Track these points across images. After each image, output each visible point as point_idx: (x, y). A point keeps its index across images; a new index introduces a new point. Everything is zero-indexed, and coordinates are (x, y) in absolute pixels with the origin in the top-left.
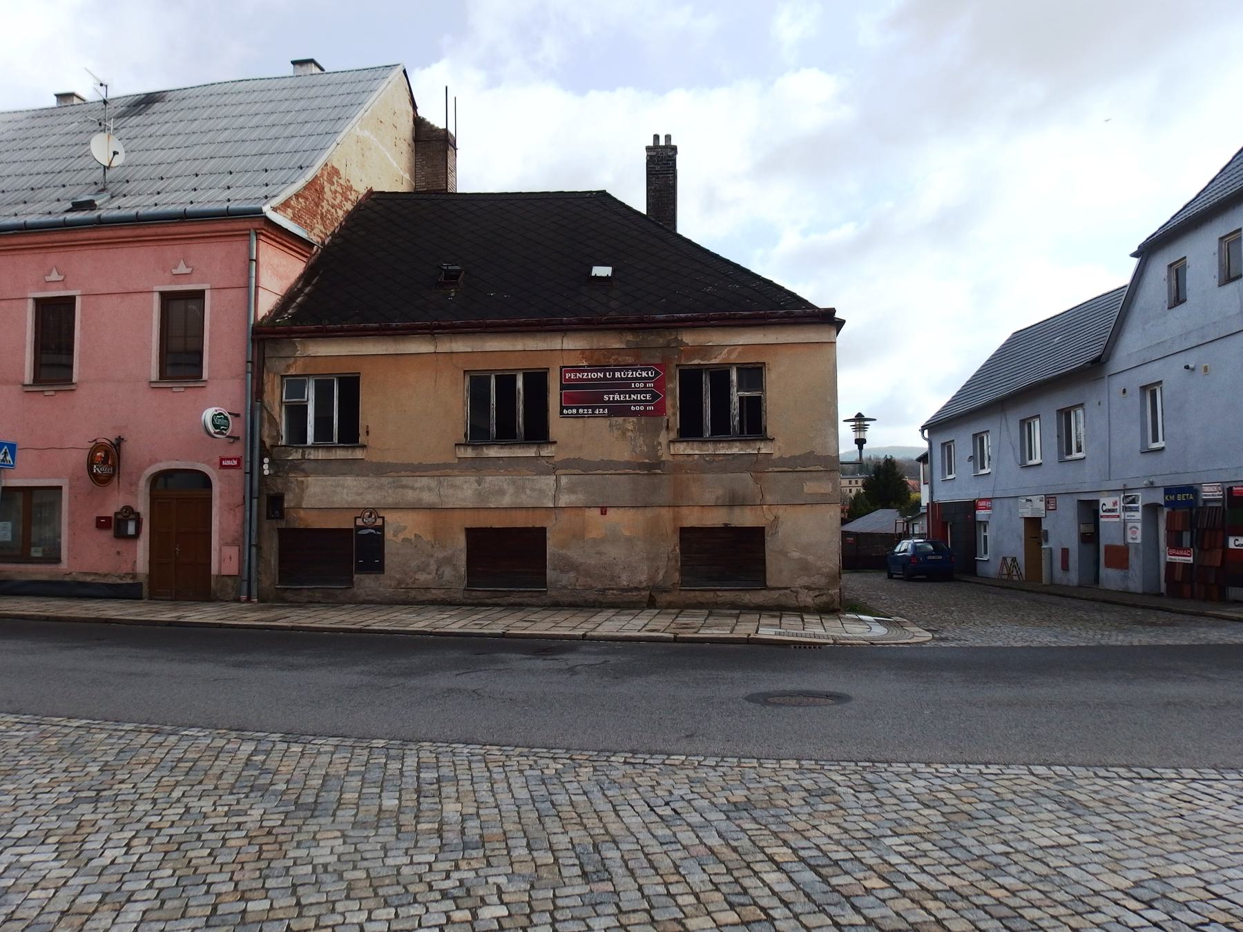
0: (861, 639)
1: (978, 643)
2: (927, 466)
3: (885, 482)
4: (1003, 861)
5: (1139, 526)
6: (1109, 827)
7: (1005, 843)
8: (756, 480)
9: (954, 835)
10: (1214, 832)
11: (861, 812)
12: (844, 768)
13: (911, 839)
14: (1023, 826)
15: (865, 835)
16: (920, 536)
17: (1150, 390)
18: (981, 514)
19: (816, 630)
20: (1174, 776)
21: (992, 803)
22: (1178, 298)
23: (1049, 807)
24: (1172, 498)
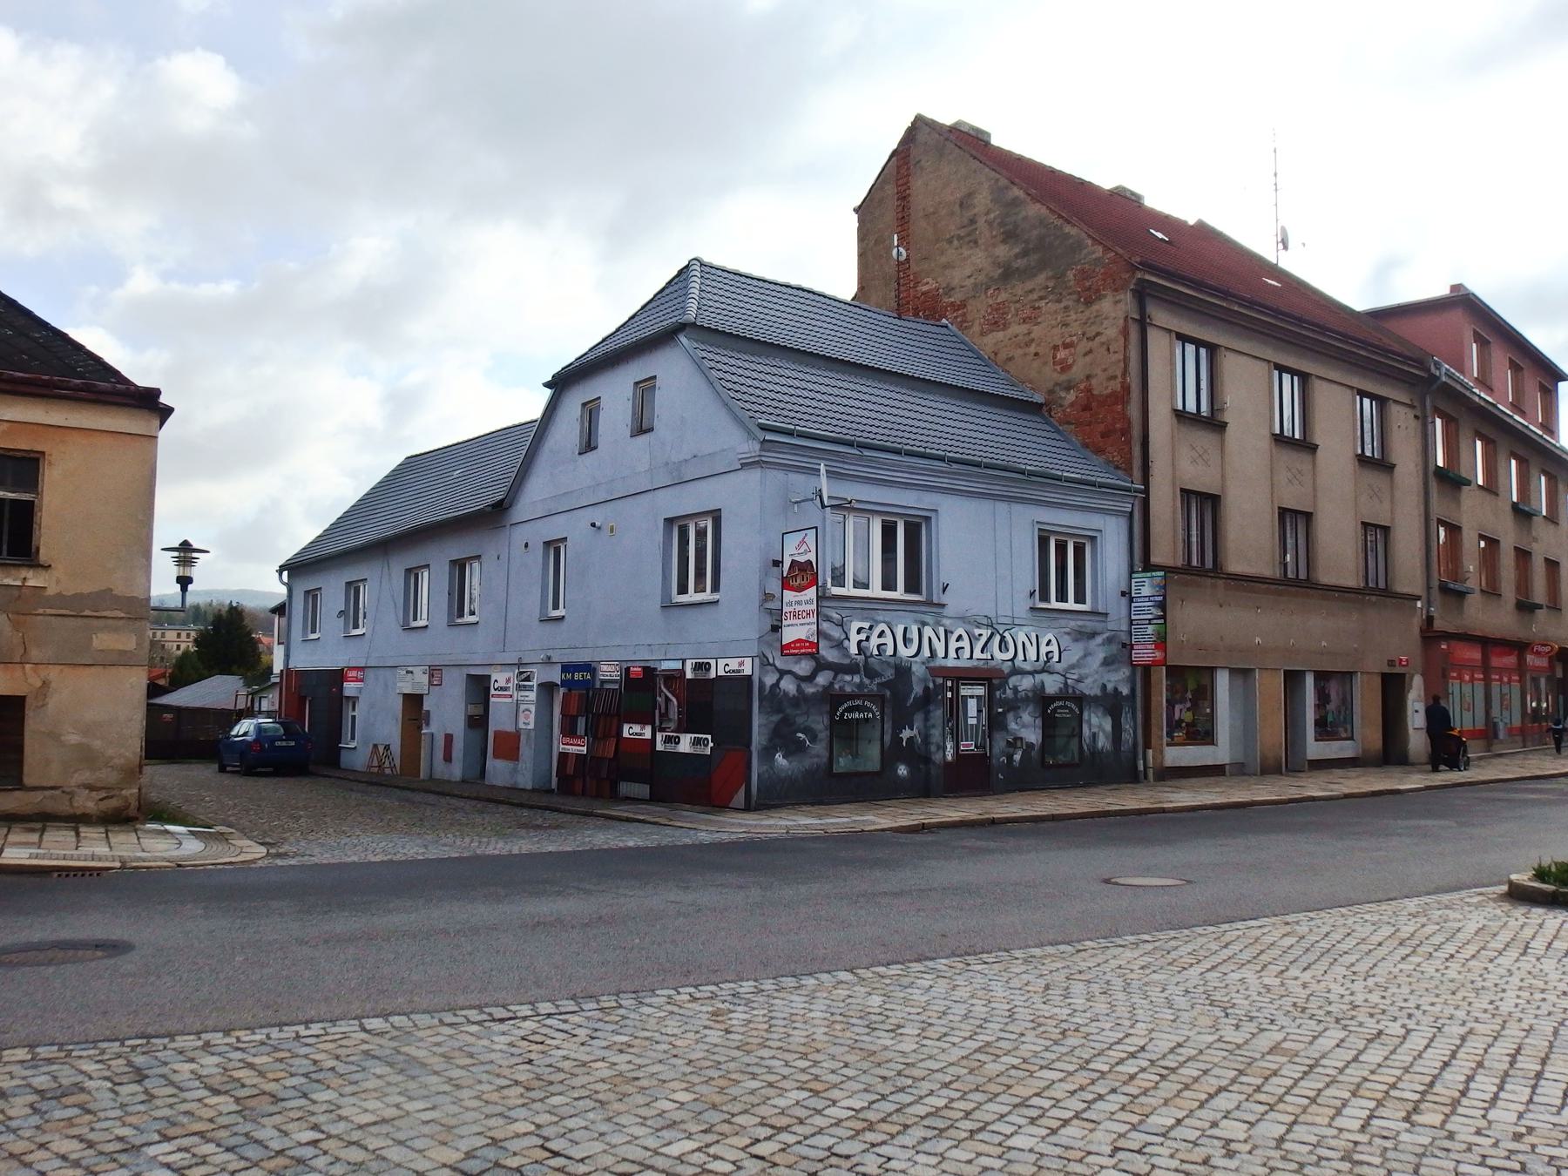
0: (164, 859)
1: (327, 858)
2: (284, 620)
3: (228, 638)
4: (308, 1152)
5: (533, 708)
6: (447, 1088)
7: (316, 1127)
8: (16, 626)
9: (248, 1127)
10: (562, 1076)
11: (118, 1113)
12: (103, 1052)
13: (186, 1142)
14: (342, 1101)
15: (119, 1146)
16: (269, 714)
17: (554, 547)
18: (350, 688)
19: (97, 849)
20: (530, 1013)
21: (306, 1075)
22: (589, 446)
23: (378, 1071)
24: (569, 676)
